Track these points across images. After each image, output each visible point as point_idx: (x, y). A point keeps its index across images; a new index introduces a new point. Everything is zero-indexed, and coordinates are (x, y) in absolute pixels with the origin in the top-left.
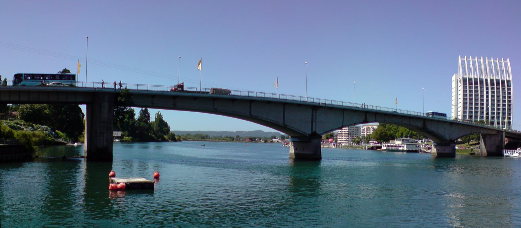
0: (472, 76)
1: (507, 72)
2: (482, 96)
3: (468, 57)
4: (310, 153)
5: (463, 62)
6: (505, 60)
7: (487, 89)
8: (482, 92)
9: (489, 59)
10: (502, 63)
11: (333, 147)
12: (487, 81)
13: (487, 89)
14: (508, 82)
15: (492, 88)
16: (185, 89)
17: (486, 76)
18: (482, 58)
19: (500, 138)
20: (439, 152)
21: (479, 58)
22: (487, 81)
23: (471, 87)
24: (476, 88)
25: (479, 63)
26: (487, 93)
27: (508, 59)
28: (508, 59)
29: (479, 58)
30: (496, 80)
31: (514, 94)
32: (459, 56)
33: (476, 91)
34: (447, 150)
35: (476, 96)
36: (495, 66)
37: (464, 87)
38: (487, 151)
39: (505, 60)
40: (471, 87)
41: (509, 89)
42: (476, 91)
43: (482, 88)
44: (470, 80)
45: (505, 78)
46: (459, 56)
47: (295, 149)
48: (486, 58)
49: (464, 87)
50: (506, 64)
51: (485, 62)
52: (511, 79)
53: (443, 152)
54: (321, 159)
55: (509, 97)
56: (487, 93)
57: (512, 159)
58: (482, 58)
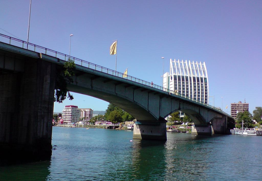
0: (181, 75)
1: (204, 72)
2: (187, 89)
3: (177, 60)
4: (159, 135)
5: (173, 64)
6: (202, 63)
7: (191, 84)
8: (187, 86)
9: (191, 62)
10: (182, 63)
11: (73, 126)
12: (190, 78)
13: (191, 84)
14: (205, 79)
15: (195, 84)
16: (78, 85)
17: (190, 75)
18: (186, 61)
19: (224, 121)
20: (199, 131)
21: (184, 61)
22: (190, 78)
23: (179, 82)
24: (183, 83)
25: (185, 64)
26: (191, 87)
27: (204, 63)
28: (204, 63)
29: (184, 61)
30: (201, 78)
31: (209, 88)
32: (171, 60)
33: (183, 86)
34: (206, 130)
35: (183, 89)
36: (177, 66)
37: (175, 82)
38: (214, 132)
39: (202, 63)
40: (179, 82)
41: (206, 84)
42: (183, 86)
43: (187, 83)
44: (179, 77)
45: (203, 76)
46: (171, 60)
47: (142, 131)
48: (189, 61)
49: (175, 82)
50: (203, 66)
51: (188, 64)
52: (207, 77)
53: (203, 132)
54: (166, 140)
55: (206, 90)
56: (191, 87)
57: (241, 136)
58: (186, 61)
